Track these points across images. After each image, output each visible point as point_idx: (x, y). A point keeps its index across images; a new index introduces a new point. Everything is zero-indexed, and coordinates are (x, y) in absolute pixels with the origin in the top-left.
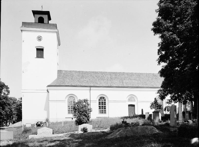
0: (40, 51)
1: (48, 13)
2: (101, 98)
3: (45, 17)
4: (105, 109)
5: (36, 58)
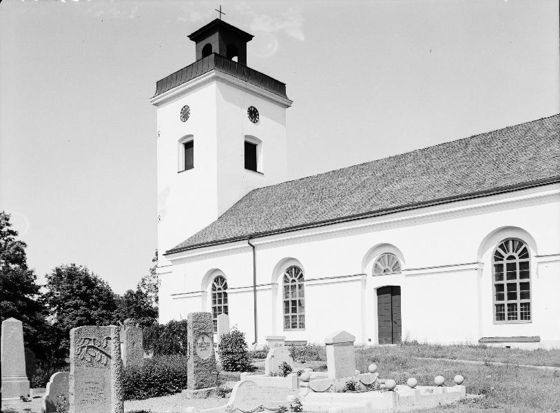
2: (504, 246)
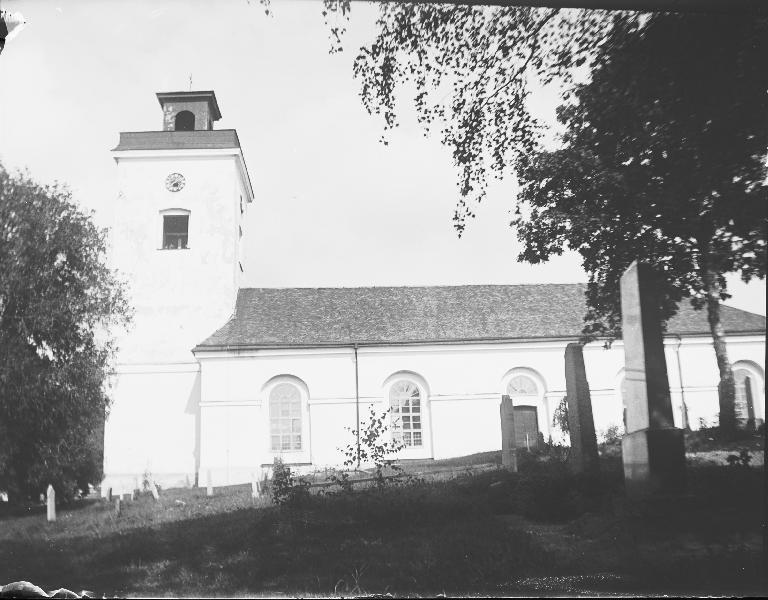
0: (176, 230)
1: (210, 98)
3: (436, 82)
4: (417, 426)
5: (164, 248)
